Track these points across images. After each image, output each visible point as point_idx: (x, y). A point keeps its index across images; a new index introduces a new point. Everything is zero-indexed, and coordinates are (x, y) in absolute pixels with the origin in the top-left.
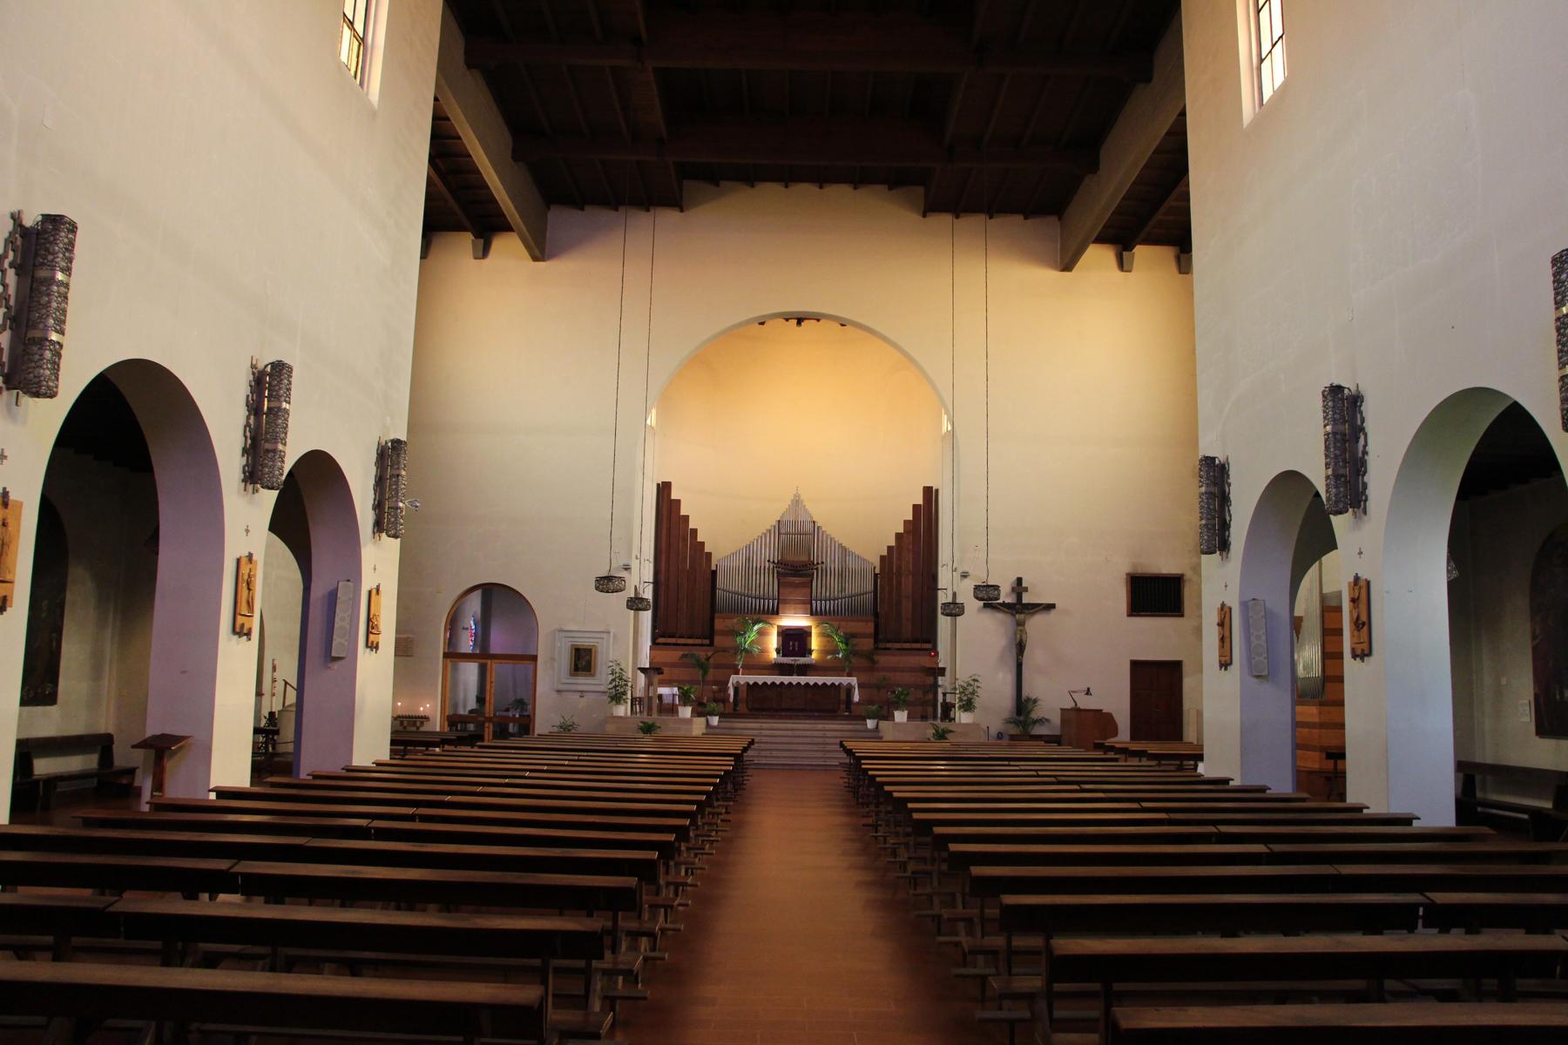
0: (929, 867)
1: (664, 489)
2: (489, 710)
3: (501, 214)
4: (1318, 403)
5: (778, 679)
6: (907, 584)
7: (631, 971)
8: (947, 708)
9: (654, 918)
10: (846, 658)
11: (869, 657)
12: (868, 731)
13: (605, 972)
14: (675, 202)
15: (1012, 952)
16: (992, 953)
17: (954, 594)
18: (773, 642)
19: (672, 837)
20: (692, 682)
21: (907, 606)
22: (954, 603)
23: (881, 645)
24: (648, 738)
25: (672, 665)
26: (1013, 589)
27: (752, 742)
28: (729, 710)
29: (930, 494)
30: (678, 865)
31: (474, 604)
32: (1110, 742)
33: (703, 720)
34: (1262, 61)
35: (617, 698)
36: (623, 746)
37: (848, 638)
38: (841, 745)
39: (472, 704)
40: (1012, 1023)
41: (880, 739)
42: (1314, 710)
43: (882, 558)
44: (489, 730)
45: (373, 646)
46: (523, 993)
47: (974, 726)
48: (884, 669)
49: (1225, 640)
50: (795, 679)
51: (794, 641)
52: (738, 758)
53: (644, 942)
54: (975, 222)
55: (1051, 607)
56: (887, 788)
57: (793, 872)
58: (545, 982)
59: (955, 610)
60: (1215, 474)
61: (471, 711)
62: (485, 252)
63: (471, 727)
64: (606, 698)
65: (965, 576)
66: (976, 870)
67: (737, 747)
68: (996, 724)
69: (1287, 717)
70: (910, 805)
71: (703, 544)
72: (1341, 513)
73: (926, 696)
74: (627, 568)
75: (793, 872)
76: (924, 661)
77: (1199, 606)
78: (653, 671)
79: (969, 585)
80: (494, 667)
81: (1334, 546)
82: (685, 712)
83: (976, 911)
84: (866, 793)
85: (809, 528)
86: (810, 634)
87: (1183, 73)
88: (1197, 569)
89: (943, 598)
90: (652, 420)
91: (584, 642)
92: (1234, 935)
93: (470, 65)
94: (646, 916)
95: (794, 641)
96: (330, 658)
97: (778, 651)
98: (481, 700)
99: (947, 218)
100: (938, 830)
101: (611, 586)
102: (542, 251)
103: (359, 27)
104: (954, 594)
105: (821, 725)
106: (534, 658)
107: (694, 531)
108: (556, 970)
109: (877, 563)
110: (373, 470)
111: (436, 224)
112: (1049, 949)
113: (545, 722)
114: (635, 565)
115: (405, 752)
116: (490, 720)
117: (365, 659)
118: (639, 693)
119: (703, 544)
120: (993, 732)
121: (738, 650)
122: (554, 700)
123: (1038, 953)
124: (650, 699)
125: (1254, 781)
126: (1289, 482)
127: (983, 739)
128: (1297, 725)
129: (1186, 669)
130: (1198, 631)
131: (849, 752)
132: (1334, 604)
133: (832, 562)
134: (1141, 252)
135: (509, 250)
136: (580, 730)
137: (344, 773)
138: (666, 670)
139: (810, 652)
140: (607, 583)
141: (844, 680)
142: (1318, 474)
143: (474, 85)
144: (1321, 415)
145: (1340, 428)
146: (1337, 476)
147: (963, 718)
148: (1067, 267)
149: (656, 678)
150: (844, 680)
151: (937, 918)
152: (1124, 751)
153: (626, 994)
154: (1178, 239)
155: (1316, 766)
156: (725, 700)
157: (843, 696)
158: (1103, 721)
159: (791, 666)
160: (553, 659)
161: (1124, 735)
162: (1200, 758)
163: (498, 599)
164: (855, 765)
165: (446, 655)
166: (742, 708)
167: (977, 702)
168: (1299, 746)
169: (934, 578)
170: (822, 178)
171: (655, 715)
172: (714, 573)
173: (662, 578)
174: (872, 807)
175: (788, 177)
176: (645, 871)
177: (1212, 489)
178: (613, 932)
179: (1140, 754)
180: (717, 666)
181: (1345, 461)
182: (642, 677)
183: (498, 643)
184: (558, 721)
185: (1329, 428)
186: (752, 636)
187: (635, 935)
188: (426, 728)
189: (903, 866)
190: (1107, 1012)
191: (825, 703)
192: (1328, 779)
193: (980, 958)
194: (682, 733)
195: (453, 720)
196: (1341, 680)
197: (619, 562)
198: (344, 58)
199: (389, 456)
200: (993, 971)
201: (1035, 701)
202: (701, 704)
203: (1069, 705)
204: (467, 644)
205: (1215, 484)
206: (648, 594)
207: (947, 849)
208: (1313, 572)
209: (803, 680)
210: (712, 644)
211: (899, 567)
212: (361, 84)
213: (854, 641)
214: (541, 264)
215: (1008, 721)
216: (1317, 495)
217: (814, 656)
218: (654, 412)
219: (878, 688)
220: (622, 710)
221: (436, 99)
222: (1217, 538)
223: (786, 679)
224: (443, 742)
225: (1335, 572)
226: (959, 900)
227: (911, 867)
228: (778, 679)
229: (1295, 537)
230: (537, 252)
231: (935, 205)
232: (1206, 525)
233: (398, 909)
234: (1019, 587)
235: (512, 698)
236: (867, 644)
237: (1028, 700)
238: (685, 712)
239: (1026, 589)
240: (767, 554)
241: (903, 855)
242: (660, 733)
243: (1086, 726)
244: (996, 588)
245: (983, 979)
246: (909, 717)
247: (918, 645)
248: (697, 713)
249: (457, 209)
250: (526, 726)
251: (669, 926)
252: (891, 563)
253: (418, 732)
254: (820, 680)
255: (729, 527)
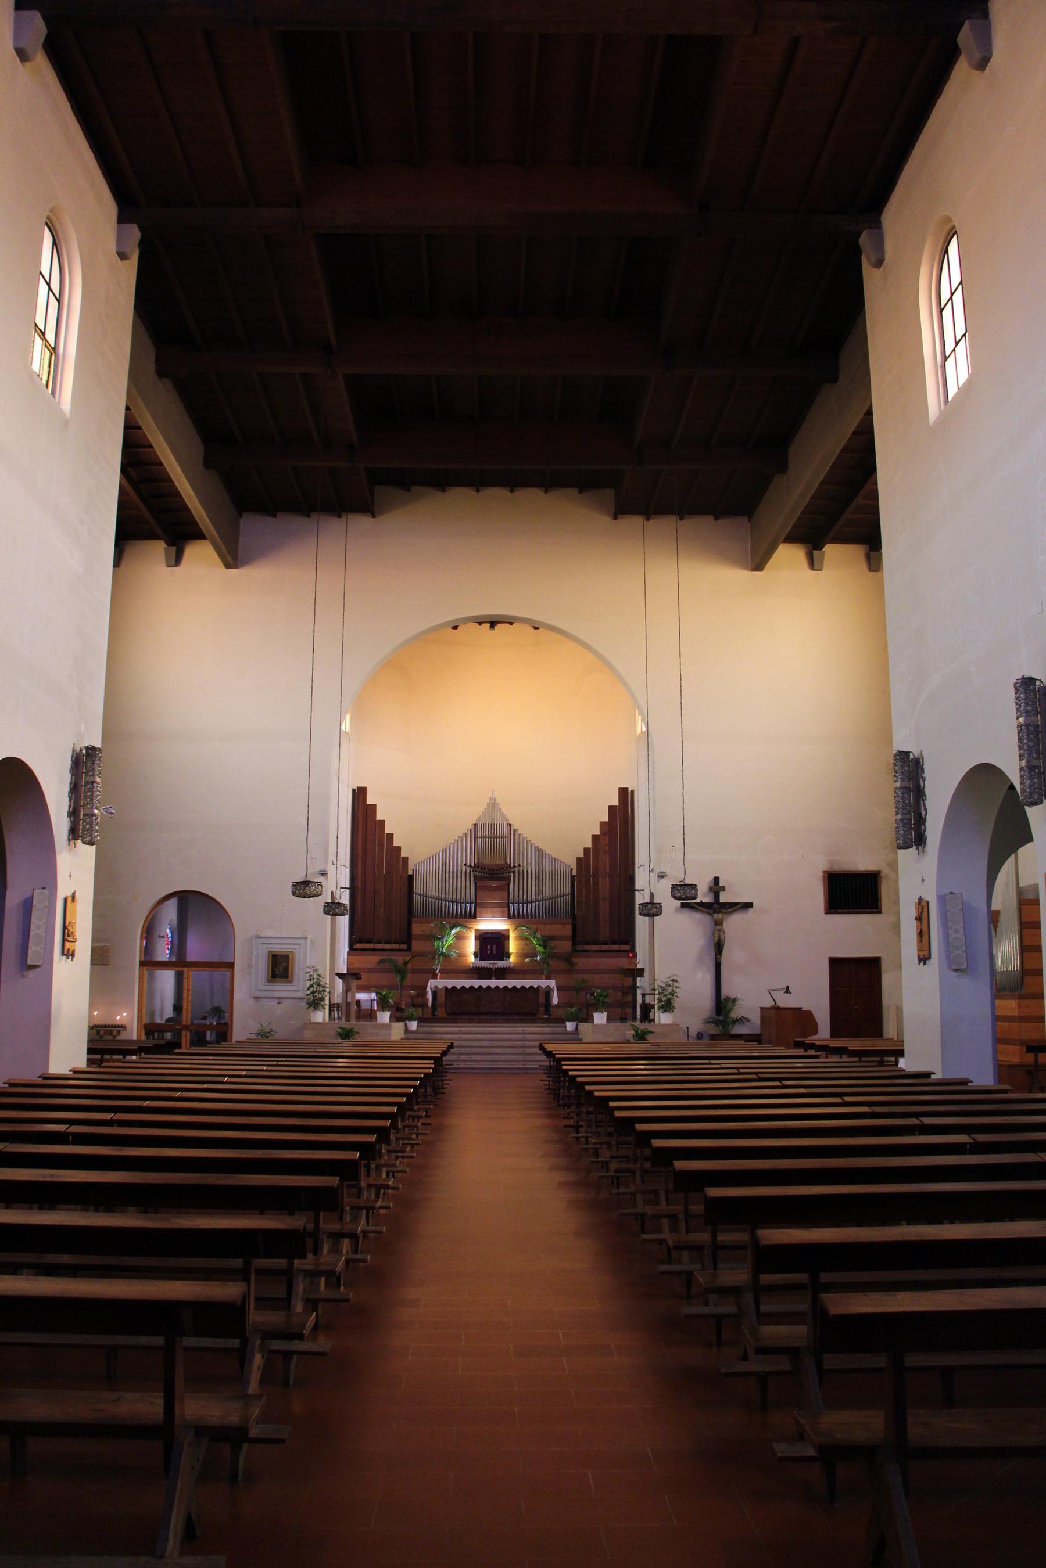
0: (631, 1166)
1: (359, 794)
2: (186, 1018)
3: (193, 522)
4: (1010, 696)
5: (476, 983)
6: (604, 885)
7: (334, 1272)
8: (647, 1009)
9: (355, 1219)
10: (544, 961)
11: (568, 959)
12: (567, 1033)
13: (308, 1274)
14: (367, 507)
15: (717, 1248)
16: (698, 1248)
17: (652, 895)
18: (470, 946)
19: (373, 1138)
20: (390, 988)
21: (604, 908)
22: (652, 903)
23: (580, 947)
24: (346, 1043)
25: (369, 971)
26: (711, 889)
27: (451, 1046)
28: (428, 1014)
29: (625, 795)
30: (379, 1167)
31: (170, 913)
32: (810, 1039)
33: (401, 1024)
34: (945, 358)
35: (315, 1004)
36: (322, 1051)
37: (545, 942)
38: (541, 1047)
39: (169, 1013)
40: (719, 1318)
41: (580, 1041)
42: (1013, 1003)
43: (579, 860)
44: (186, 1038)
45: (69, 954)
46: (228, 1291)
47: (674, 1027)
48: (586, 972)
49: (923, 935)
50: (493, 983)
51: (492, 944)
52: (437, 1061)
53: (346, 1243)
54: (666, 524)
55: (749, 905)
56: (588, 1088)
57: (496, 1197)
58: (247, 1279)
59: (652, 910)
60: (910, 770)
61: (168, 1020)
62: (177, 560)
63: (168, 1036)
64: (304, 1004)
65: (662, 876)
66: (680, 1165)
67: (436, 1050)
68: (696, 1025)
69: (987, 1011)
70: (612, 1104)
71: (399, 849)
72: (1036, 804)
73: (626, 998)
74: (324, 873)
75: (496, 1197)
76: (623, 962)
77: (896, 903)
78: (350, 976)
79: (666, 885)
80: (191, 974)
81: (1030, 839)
82: (384, 1017)
83: (680, 1207)
84: (569, 1097)
85: (505, 831)
86: (508, 938)
87: (867, 373)
88: (893, 865)
89: (640, 899)
90: (347, 725)
91: (280, 948)
92: (939, 1222)
93: (161, 373)
94: (348, 1218)
95: (492, 944)
96: (25, 967)
97: (476, 955)
98: (178, 1008)
99: (637, 520)
100: (640, 1127)
101: (308, 891)
102: (235, 558)
103: (50, 337)
104: (652, 895)
105: (520, 1028)
106: (231, 965)
107: (390, 836)
108: (259, 1272)
109: (574, 866)
110: (67, 778)
111: (128, 533)
112: (755, 1240)
113: (242, 1028)
114: (331, 870)
115: (102, 1060)
116: (187, 1028)
117: (61, 968)
118: (337, 999)
119: (399, 849)
120: (693, 1032)
121: (435, 954)
122: (252, 1006)
123: (743, 1247)
124: (348, 1004)
125: (956, 1073)
126: (983, 776)
127: (683, 1039)
128: (996, 1019)
129: (885, 966)
130: (896, 927)
131: (549, 1054)
132: (1031, 897)
133: (528, 864)
134: (831, 551)
135: (201, 555)
136: (277, 1036)
137: (40, 1081)
138: (364, 976)
139: (508, 955)
140: (303, 888)
141: (543, 983)
142: (1011, 765)
143: (166, 394)
144: (1014, 707)
145: (1033, 719)
146: (1031, 768)
147: (663, 1018)
148: (758, 565)
149: (354, 983)
150: (543, 983)
151: (641, 1217)
152: (824, 1048)
153: (329, 1296)
154: (868, 537)
155: (1017, 1060)
156: (424, 1005)
157: (542, 1000)
158: (803, 1019)
159: (490, 969)
160: (250, 966)
161: (824, 1033)
162: (901, 1053)
163: (195, 906)
164: (556, 1069)
165: (142, 964)
166: (441, 1012)
167: (676, 1002)
168: (999, 1040)
169: (631, 879)
170: (513, 482)
171: (353, 1021)
172: (411, 877)
173: (359, 884)
174: (573, 1108)
175: (478, 481)
176: (346, 1170)
177: (906, 784)
178: (315, 1234)
179: (841, 1051)
180: (415, 971)
181: (1038, 752)
182: (339, 982)
183: (193, 954)
184: (256, 1027)
185: (1021, 720)
186: (450, 940)
187: (336, 1237)
188: (123, 1036)
189: (605, 1166)
190: (815, 1302)
191: (524, 1007)
192: (1029, 1072)
193: (685, 1254)
194: (380, 1038)
195: (150, 1029)
196: (1039, 972)
197: (315, 867)
198: (35, 367)
199: (84, 763)
200: (699, 1266)
201: (734, 1000)
202: (399, 1009)
203: (768, 1003)
204: (163, 952)
205: (910, 779)
206: (345, 899)
207: (649, 1145)
208: (1010, 861)
209: (502, 983)
210: (409, 949)
211: (596, 869)
212: (53, 393)
213: (553, 943)
214: (234, 572)
215: (707, 1021)
216: (1012, 787)
217: (512, 959)
218: (348, 717)
219: (578, 990)
220: (320, 1016)
221: (127, 408)
222: (912, 832)
223: (485, 983)
224: (141, 1050)
225: (1030, 864)
226: (663, 1197)
227: (613, 1166)
228: (476, 983)
229: (994, 816)
230: (230, 560)
231: (622, 509)
232: (902, 820)
233: (97, 1210)
234: (716, 887)
235: (209, 1007)
236: (566, 946)
237: (728, 999)
238: (384, 1017)
239: (723, 889)
240: (464, 858)
241: (605, 1155)
242: (358, 1039)
243: (786, 1024)
244: (693, 887)
245: (689, 1275)
246: (609, 1019)
247: (616, 947)
248: (395, 1018)
249: (149, 518)
250: (223, 1033)
251: (370, 1228)
252: (588, 864)
253: (115, 1040)
254: (518, 983)
255: (426, 831)
